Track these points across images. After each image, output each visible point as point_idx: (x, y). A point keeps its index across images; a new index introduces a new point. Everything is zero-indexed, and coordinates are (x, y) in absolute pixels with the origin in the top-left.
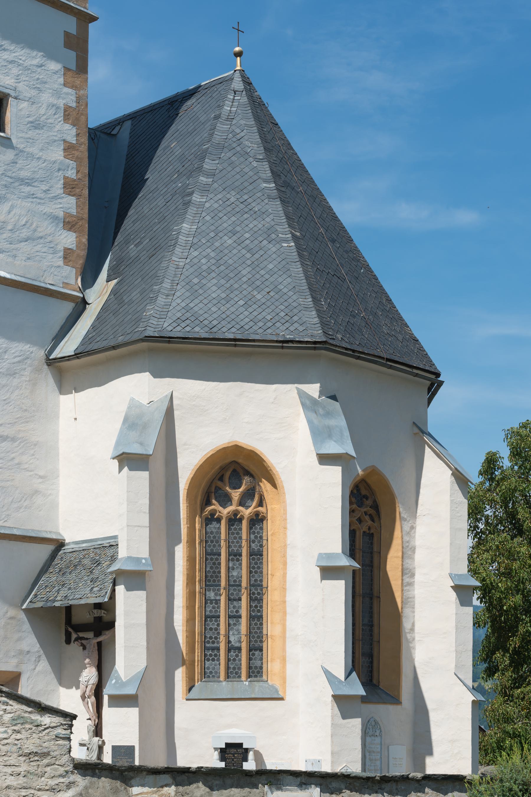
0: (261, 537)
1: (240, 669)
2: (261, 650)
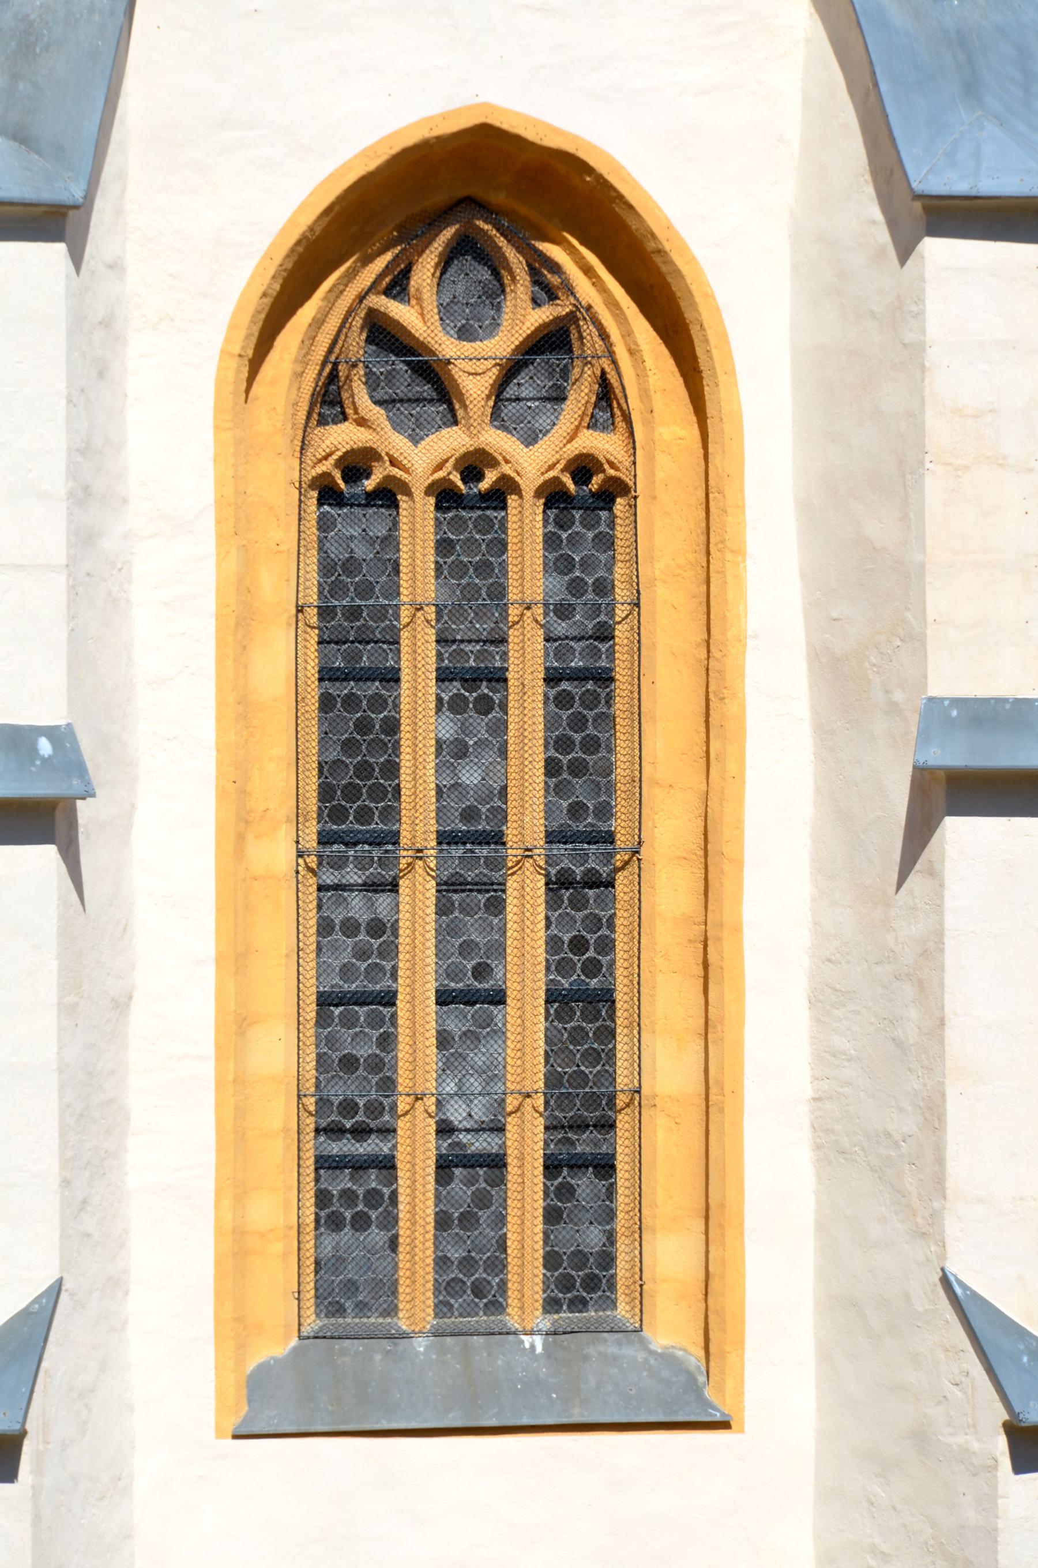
0: (604, 587)
1: (498, 1264)
2: (605, 1167)
